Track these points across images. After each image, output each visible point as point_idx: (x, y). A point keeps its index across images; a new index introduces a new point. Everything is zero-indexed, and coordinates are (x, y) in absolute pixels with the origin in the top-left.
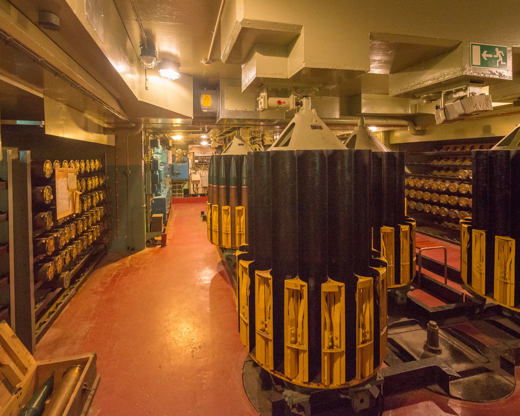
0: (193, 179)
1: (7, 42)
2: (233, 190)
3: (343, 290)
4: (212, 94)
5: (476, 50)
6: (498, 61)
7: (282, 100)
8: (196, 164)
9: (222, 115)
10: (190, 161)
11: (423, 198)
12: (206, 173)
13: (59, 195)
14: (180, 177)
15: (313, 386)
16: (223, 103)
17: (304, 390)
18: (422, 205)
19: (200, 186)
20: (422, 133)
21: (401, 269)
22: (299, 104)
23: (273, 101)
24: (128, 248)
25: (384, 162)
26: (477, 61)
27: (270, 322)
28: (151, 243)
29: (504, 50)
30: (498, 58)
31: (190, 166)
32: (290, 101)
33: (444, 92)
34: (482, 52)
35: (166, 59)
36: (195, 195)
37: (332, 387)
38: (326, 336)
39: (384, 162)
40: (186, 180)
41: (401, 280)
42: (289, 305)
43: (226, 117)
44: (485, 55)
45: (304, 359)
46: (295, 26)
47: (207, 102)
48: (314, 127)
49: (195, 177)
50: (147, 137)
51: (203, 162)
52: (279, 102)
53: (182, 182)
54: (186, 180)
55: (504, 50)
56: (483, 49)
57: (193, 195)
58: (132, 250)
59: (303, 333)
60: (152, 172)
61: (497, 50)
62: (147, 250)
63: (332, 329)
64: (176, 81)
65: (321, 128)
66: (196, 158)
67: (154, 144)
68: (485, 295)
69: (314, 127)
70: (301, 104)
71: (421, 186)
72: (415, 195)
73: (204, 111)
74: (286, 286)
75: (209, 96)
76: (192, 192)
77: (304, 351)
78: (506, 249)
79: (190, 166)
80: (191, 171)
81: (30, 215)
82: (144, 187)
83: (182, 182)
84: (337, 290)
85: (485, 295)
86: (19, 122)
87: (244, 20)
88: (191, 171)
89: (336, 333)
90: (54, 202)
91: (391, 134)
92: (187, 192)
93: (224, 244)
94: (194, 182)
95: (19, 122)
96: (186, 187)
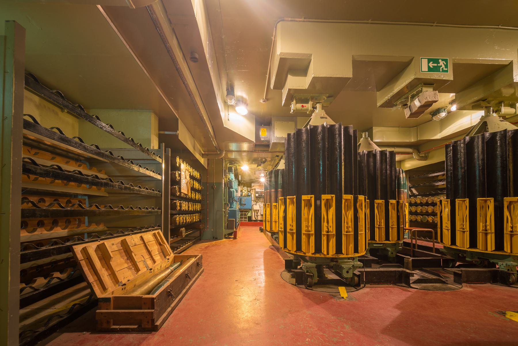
0: (255, 209)
1: (177, 69)
2: (280, 192)
3: (334, 198)
4: (267, 128)
5: (425, 62)
6: (441, 68)
7: (304, 105)
8: (257, 197)
9: (273, 140)
10: (253, 195)
11: (427, 212)
12: (262, 205)
13: (182, 179)
14: (245, 207)
15: (318, 255)
16: (274, 134)
17: (312, 260)
18: (427, 217)
19: (259, 214)
20: (425, 158)
21: (390, 230)
22: (314, 108)
23: (299, 106)
24: (214, 238)
25: (378, 157)
26: (425, 68)
27: (294, 224)
28: (228, 236)
29: (446, 61)
30: (441, 66)
31: (253, 199)
32: (309, 106)
33: (410, 96)
34: (429, 63)
35: (241, 100)
36: (256, 221)
37: (327, 256)
38: (324, 225)
39: (378, 157)
40: (250, 210)
41: (390, 238)
42: (304, 211)
43: (275, 141)
44: (431, 65)
45: (312, 239)
46: (308, 54)
47: (264, 134)
48: (322, 118)
49: (256, 207)
50: (226, 165)
51: (261, 196)
52: (303, 106)
53: (247, 211)
54: (250, 210)
55: (446, 61)
56: (429, 61)
57: (255, 221)
58: (215, 238)
59: (311, 224)
60: (229, 189)
61: (440, 61)
62: (224, 240)
63: (328, 222)
64: (245, 116)
65: (326, 118)
66: (257, 193)
67: (230, 170)
68: (451, 245)
69: (322, 118)
70: (316, 108)
71: (425, 201)
72: (421, 210)
73: (262, 139)
74: (303, 198)
75: (265, 129)
76: (254, 219)
77: (312, 234)
78: (464, 207)
79: (253, 199)
80: (253, 203)
81: (170, 187)
82: (223, 198)
83: (247, 211)
84: (330, 198)
85: (451, 245)
86: (166, 133)
87: (281, 53)
88: (253, 203)
89: (330, 224)
90: (180, 180)
91: (402, 164)
92: (250, 218)
93: (273, 229)
94: (255, 211)
95: (166, 133)
96: (249, 215)
